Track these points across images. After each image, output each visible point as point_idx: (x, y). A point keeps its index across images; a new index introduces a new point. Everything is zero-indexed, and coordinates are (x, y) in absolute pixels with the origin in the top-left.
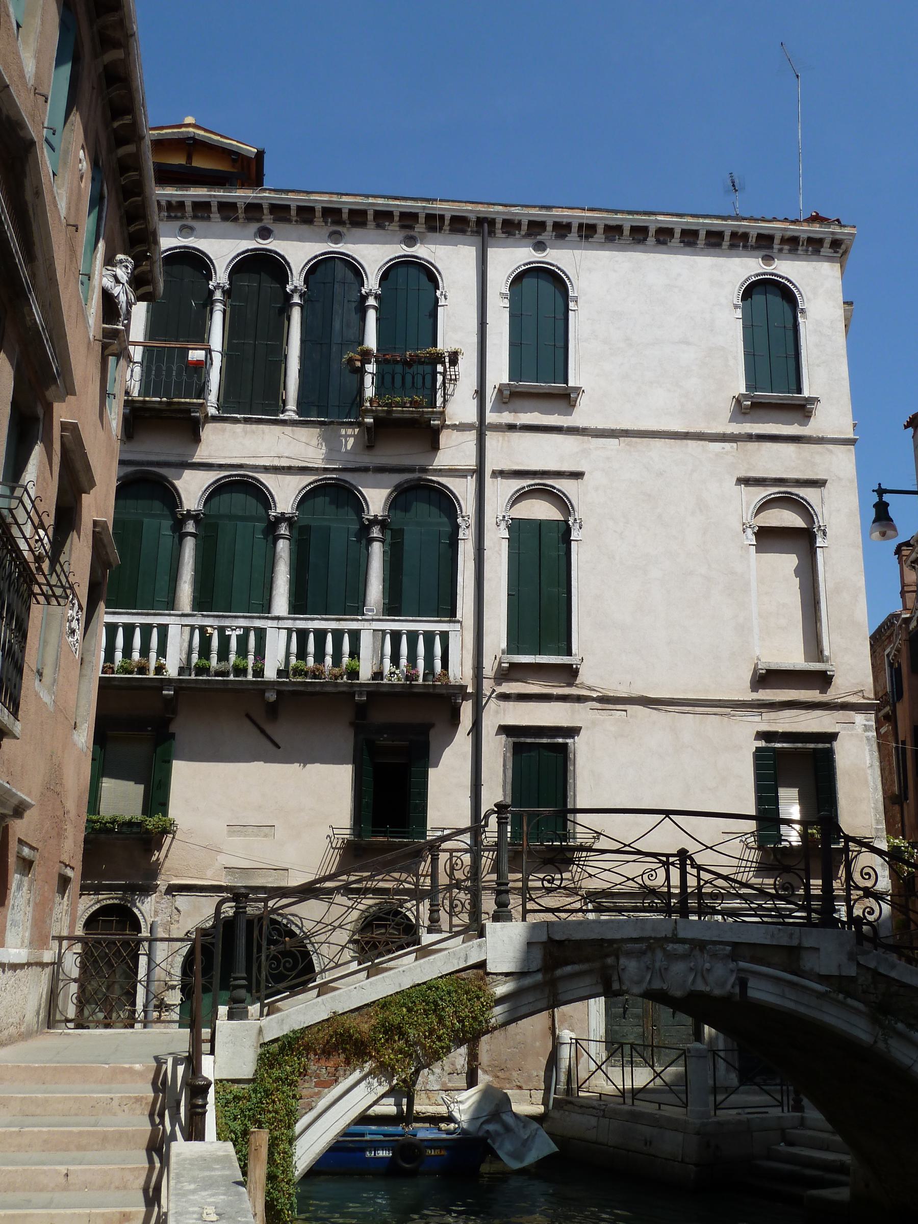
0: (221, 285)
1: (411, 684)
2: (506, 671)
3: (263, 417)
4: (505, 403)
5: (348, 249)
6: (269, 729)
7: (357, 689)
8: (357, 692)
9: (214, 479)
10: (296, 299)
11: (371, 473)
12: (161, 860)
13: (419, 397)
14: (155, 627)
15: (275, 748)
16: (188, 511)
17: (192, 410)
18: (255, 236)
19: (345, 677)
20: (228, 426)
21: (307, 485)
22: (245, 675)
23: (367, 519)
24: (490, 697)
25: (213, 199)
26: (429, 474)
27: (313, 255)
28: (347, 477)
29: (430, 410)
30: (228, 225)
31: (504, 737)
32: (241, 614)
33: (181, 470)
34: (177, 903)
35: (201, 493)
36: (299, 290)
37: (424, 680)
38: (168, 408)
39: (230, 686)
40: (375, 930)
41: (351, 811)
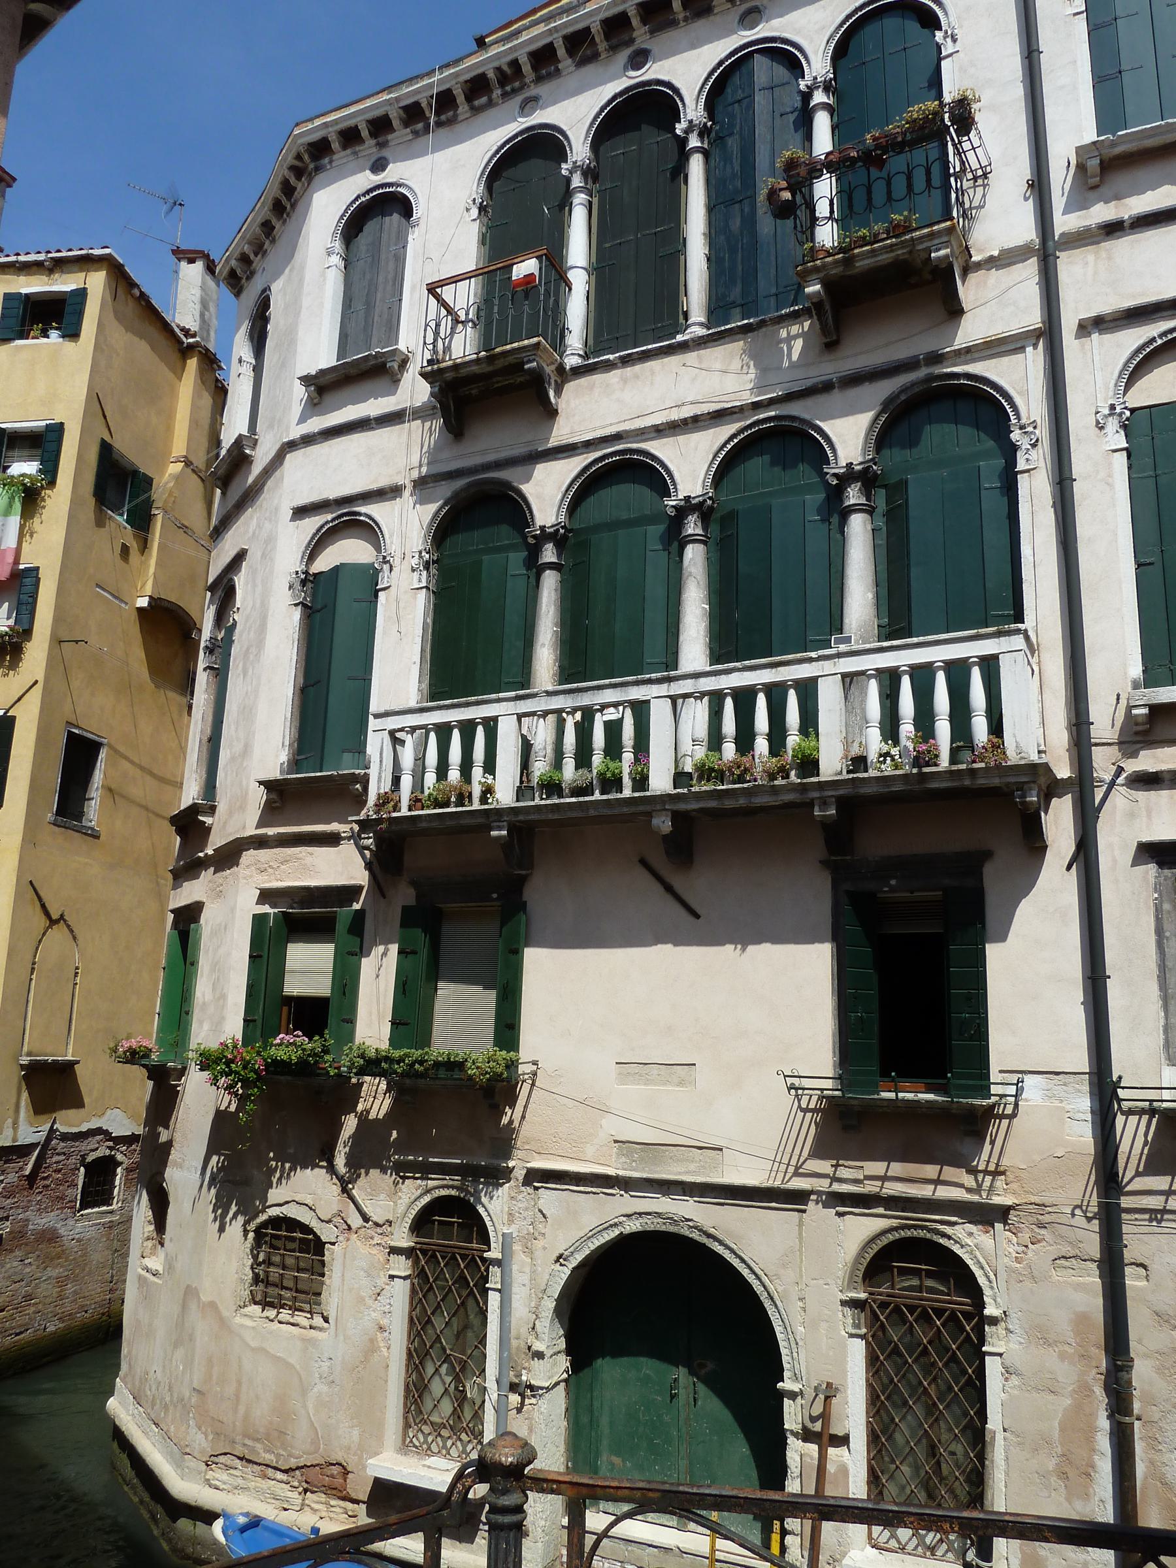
0: (578, 164)
1: (920, 774)
2: (1143, 724)
3: (650, 347)
4: (1094, 188)
5: (773, 30)
6: (677, 883)
7: (815, 794)
8: (816, 802)
9: (579, 468)
10: (694, 142)
11: (836, 390)
12: (516, 1124)
13: (901, 215)
14: (479, 723)
15: (691, 919)
16: (542, 528)
17: (525, 359)
18: (625, 69)
19: (793, 773)
20: (597, 378)
21: (727, 442)
22: (620, 789)
23: (835, 475)
24: (1112, 784)
25: (555, 35)
26: (945, 363)
27: (717, 61)
28: (795, 409)
29: (926, 231)
30: (589, 70)
31: (1151, 869)
32: (607, 681)
33: (530, 467)
34: (541, 1201)
35: (560, 496)
36: (695, 126)
37: (953, 760)
38: (491, 368)
39: (592, 812)
40: (897, 1279)
41: (834, 1035)
